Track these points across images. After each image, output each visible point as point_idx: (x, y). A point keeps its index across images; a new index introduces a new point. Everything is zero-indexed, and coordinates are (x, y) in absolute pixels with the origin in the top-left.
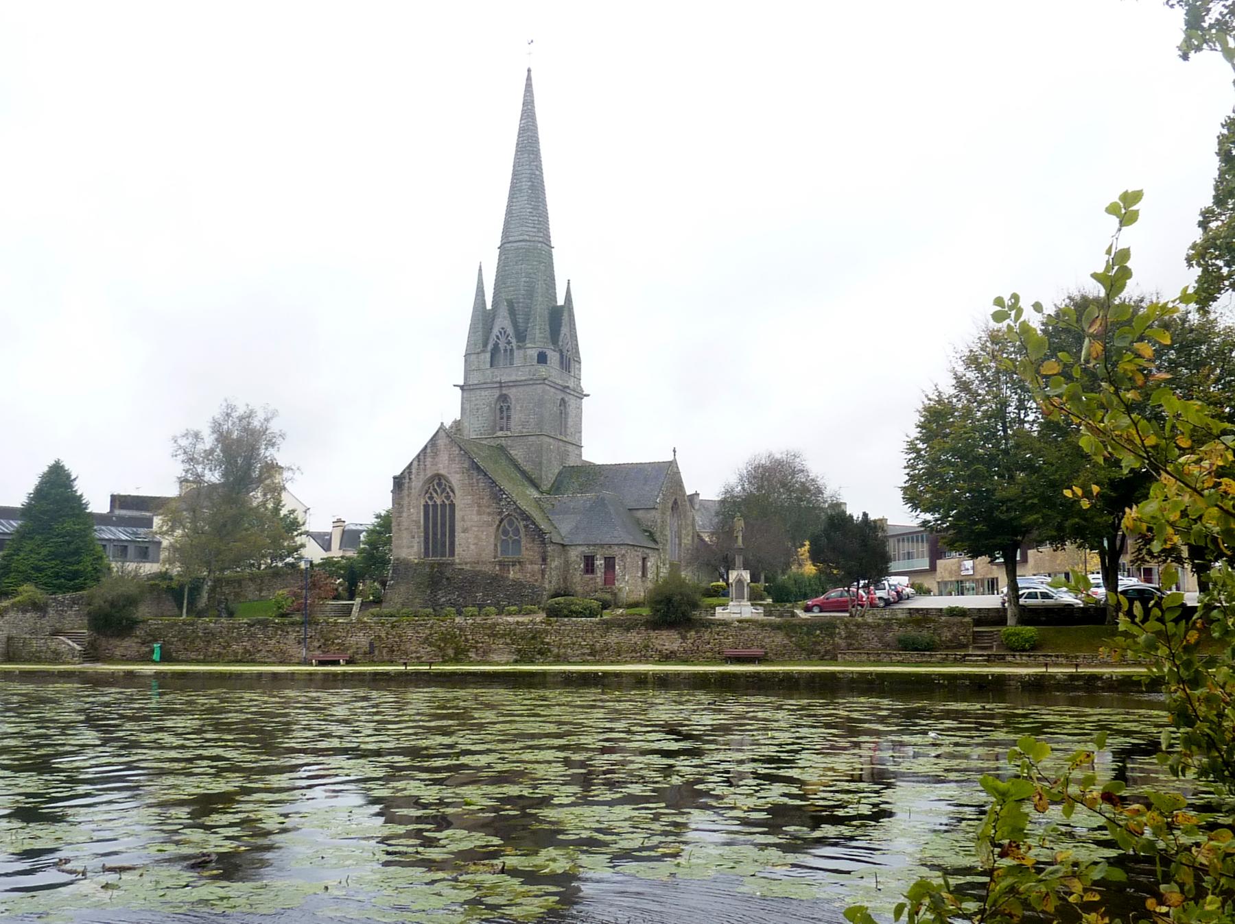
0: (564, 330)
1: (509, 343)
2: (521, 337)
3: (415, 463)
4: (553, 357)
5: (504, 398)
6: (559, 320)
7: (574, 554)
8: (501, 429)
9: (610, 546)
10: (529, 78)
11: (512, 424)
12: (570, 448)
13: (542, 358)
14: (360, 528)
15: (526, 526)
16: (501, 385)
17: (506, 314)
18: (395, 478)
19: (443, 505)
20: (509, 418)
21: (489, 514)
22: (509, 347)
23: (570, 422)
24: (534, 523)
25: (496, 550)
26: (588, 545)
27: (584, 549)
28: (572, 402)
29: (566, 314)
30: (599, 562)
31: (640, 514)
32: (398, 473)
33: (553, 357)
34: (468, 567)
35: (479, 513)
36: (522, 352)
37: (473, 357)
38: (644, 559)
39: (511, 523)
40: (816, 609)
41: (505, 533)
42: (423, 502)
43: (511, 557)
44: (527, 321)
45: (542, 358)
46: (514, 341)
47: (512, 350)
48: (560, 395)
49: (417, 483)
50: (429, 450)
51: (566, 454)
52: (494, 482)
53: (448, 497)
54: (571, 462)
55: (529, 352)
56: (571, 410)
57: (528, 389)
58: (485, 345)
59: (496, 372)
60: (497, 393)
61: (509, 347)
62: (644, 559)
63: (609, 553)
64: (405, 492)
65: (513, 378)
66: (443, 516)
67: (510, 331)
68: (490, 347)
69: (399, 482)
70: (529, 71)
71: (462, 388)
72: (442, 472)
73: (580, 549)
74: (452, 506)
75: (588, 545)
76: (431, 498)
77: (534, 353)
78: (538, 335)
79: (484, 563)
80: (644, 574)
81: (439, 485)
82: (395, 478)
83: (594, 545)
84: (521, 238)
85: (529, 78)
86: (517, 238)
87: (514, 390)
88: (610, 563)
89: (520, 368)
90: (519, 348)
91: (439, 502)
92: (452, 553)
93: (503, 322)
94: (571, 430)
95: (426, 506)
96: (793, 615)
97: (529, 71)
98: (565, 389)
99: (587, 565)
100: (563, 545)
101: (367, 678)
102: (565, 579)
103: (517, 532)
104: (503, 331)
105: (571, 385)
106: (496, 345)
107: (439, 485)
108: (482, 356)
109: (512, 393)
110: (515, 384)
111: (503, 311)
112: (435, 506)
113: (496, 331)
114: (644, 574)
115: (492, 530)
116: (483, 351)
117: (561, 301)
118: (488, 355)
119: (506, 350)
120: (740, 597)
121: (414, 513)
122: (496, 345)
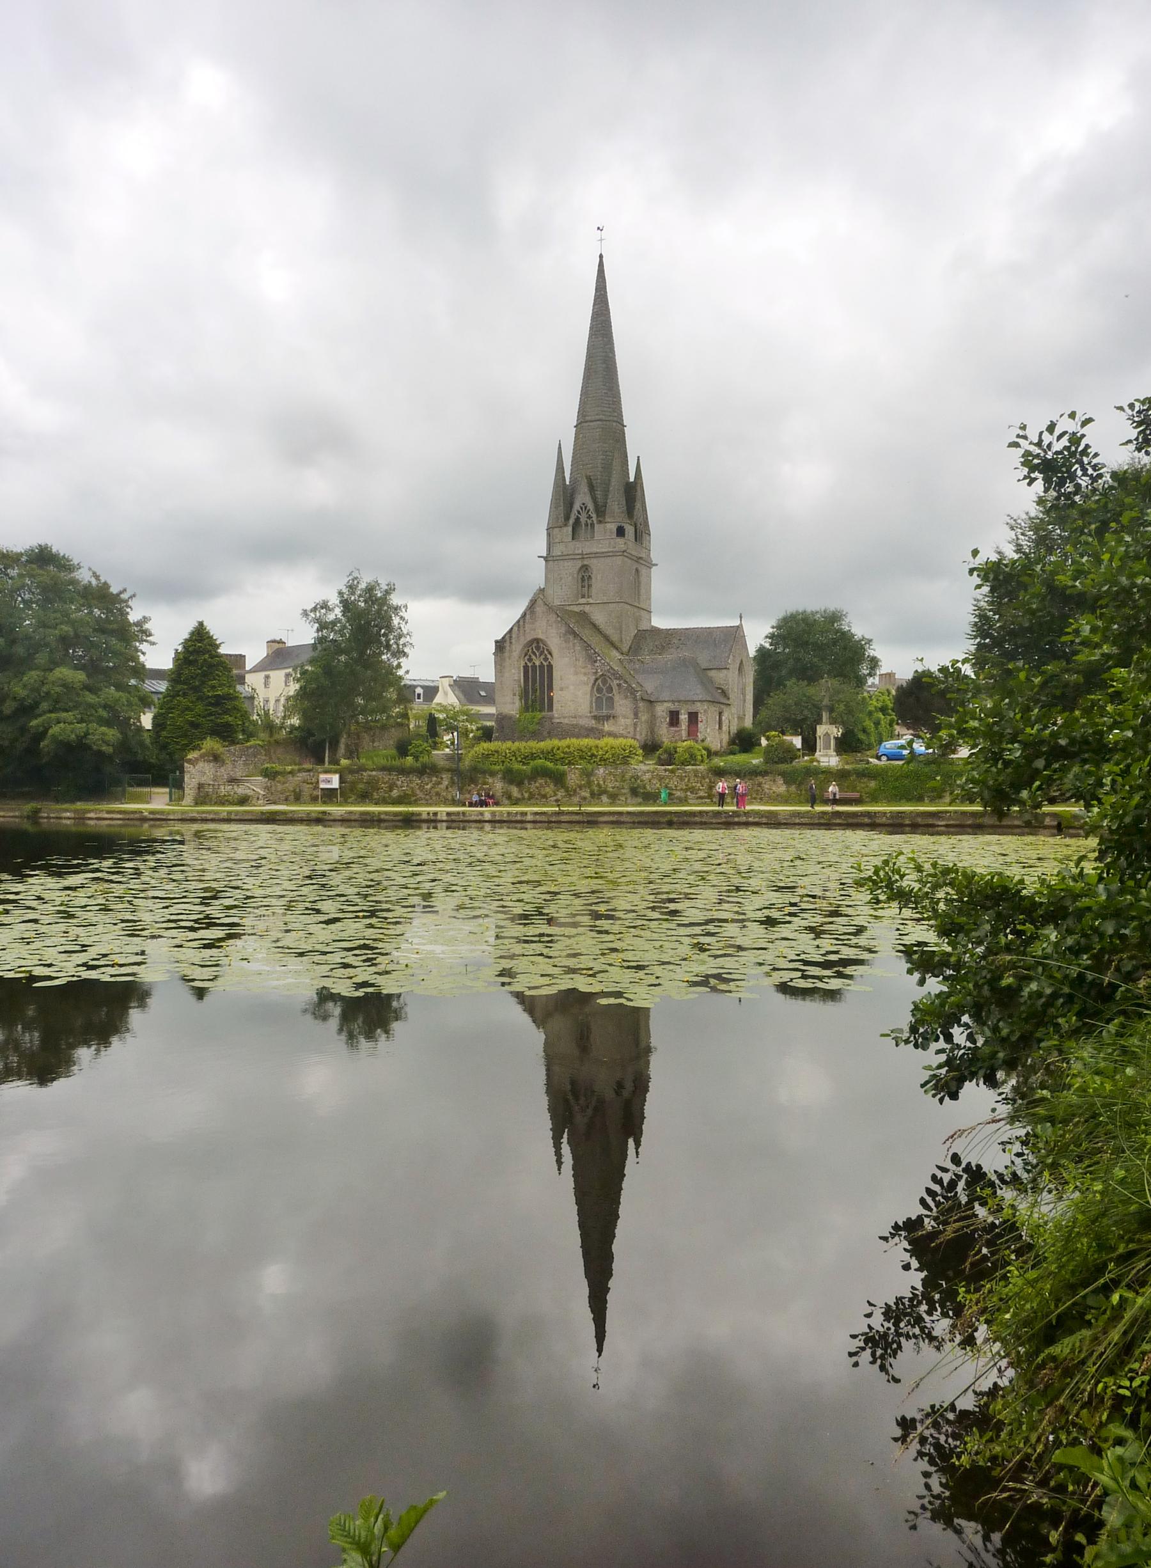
0: (638, 505)
1: (589, 517)
2: (601, 511)
3: (516, 628)
4: (629, 530)
5: (585, 568)
6: (633, 493)
7: (661, 710)
8: (583, 597)
9: (694, 702)
10: (601, 264)
11: (594, 590)
12: (643, 613)
13: (621, 532)
14: (415, 683)
15: (619, 685)
16: (583, 556)
17: (586, 490)
18: (496, 642)
19: (542, 666)
20: (589, 586)
21: (585, 674)
22: (589, 522)
23: (643, 591)
24: (626, 682)
25: (591, 707)
26: (673, 702)
27: (670, 705)
28: (643, 571)
29: (638, 488)
30: (684, 717)
31: (712, 673)
32: (499, 638)
33: (629, 530)
34: (566, 721)
35: (576, 673)
36: (602, 525)
37: (557, 530)
38: (720, 714)
39: (605, 682)
40: (884, 758)
41: (599, 690)
42: (523, 664)
43: (605, 712)
44: (606, 496)
45: (621, 532)
46: (594, 516)
47: (592, 525)
48: (635, 565)
49: (517, 649)
50: (528, 616)
51: (638, 620)
52: (589, 646)
53: (546, 659)
54: (644, 626)
55: (608, 526)
56: (643, 579)
57: (608, 560)
58: (567, 518)
59: (578, 544)
60: (579, 564)
61: (589, 522)
62: (720, 714)
63: (693, 709)
64: (507, 654)
65: (595, 550)
66: (542, 676)
67: (591, 506)
68: (571, 521)
69: (500, 646)
70: (601, 256)
71: (546, 559)
72: (540, 636)
73: (666, 704)
74: (550, 667)
75: (673, 702)
76: (530, 660)
77: (613, 527)
78: (617, 510)
79: (580, 717)
80: (720, 727)
81: (538, 648)
82: (496, 642)
83: (679, 701)
84: (597, 417)
85: (601, 264)
86: (593, 418)
87: (594, 561)
88: (693, 717)
89: (603, 538)
90: (600, 522)
91: (537, 663)
92: (551, 708)
93: (583, 498)
94: (643, 597)
95: (526, 667)
96: (868, 762)
97: (601, 256)
98: (638, 559)
99: (671, 719)
100: (651, 702)
101: (765, 799)
102: (652, 731)
103: (610, 689)
104: (584, 506)
105: (643, 555)
106: (577, 519)
107: (538, 648)
108: (565, 529)
109: (594, 563)
110: (596, 555)
111: (584, 488)
112: (534, 666)
113: (577, 507)
114: (720, 727)
115: (588, 688)
116: (566, 525)
117: (632, 479)
118: (570, 529)
119: (587, 525)
120: (827, 747)
121: (515, 674)
122: (577, 519)
